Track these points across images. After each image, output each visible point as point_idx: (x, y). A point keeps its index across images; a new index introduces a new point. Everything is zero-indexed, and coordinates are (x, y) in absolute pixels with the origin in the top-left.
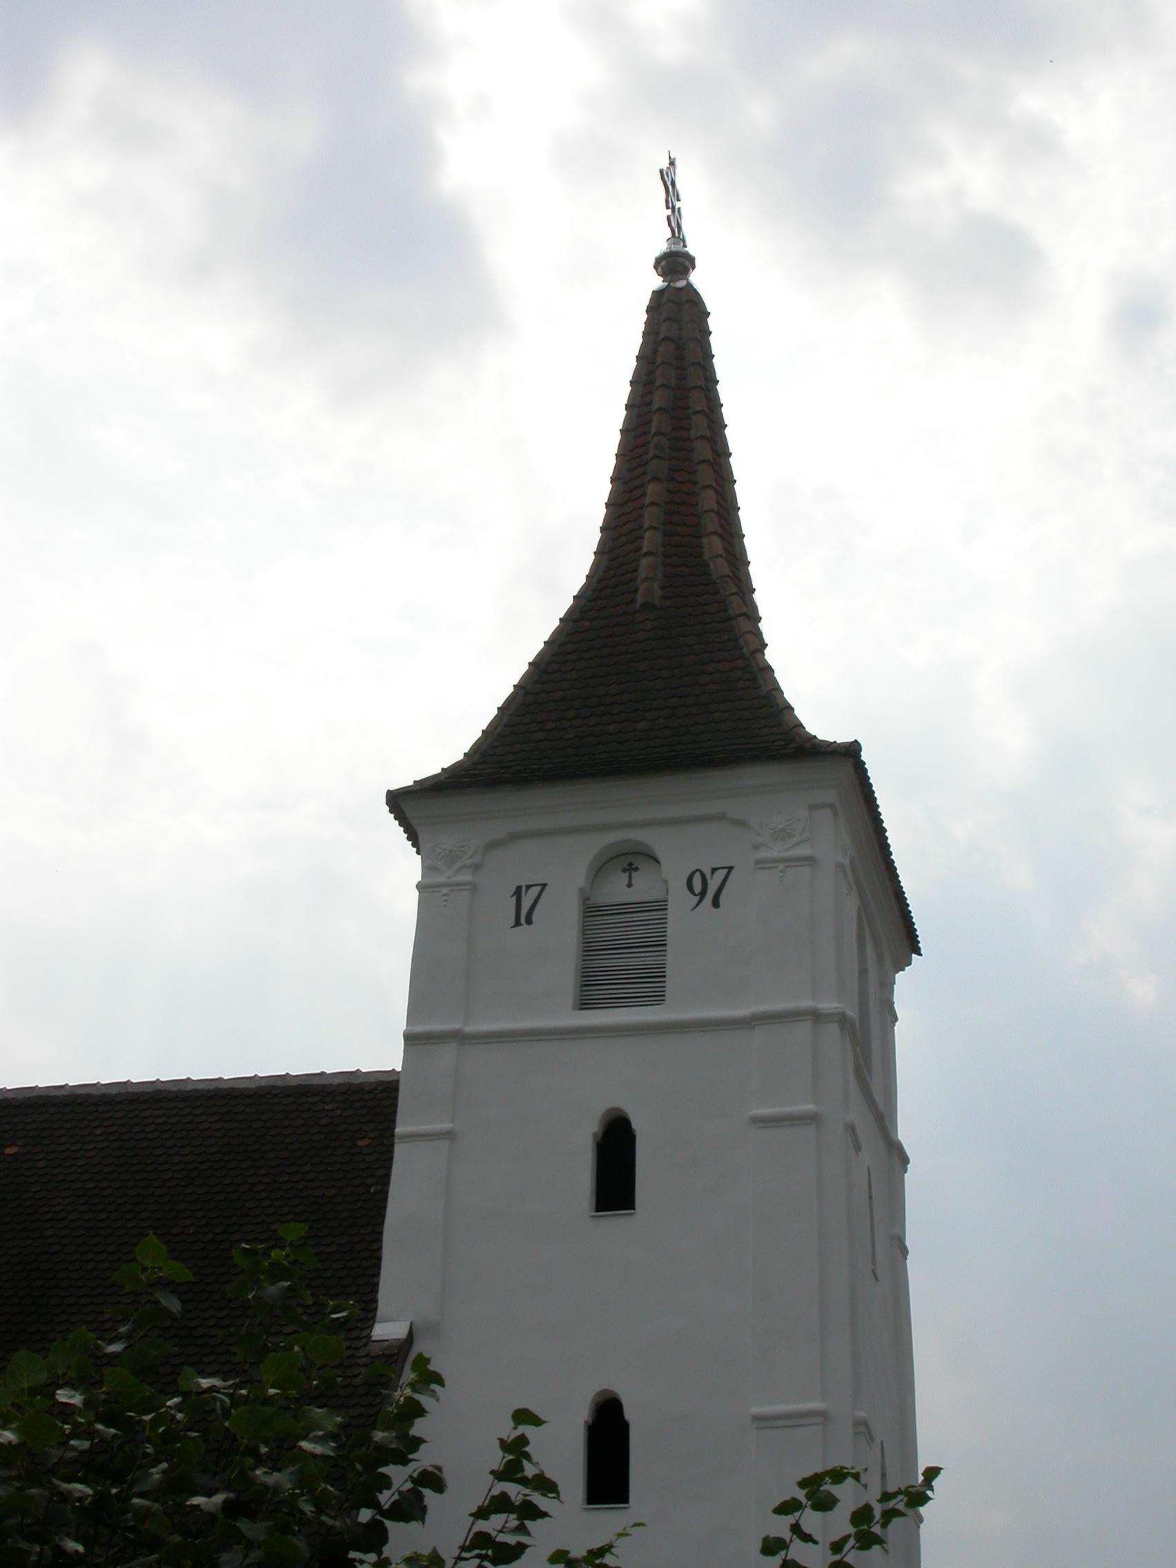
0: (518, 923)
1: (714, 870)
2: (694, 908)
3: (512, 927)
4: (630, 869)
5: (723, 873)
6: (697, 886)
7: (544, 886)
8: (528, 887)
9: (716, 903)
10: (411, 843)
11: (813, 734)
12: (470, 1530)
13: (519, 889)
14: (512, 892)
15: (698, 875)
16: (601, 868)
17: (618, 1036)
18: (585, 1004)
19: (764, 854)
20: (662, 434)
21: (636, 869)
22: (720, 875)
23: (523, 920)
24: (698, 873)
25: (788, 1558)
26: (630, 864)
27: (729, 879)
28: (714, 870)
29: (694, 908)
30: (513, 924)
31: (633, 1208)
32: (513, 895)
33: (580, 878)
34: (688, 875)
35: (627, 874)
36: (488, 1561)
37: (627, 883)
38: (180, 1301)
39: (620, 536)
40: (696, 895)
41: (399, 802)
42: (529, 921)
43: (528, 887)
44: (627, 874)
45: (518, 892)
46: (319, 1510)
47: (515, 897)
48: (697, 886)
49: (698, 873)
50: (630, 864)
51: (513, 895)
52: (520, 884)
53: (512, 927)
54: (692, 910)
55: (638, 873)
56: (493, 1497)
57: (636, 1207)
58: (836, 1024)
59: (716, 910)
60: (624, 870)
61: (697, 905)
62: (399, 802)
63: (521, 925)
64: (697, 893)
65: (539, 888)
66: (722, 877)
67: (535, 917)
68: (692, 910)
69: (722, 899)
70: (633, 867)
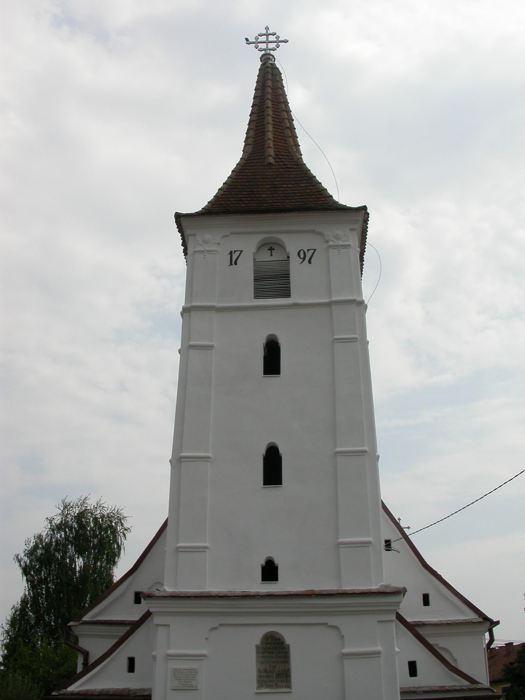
0: (231, 264)
1: (308, 250)
3: (229, 266)
4: (271, 249)
5: (312, 251)
6: (302, 256)
7: (242, 251)
8: (235, 251)
9: (310, 262)
14: (229, 252)
16: (260, 247)
17: (229, 311)
18: (257, 296)
20: (249, 144)
21: (274, 249)
22: (311, 252)
23: (233, 263)
24: (302, 251)
25: (498, 643)
26: (271, 247)
28: (308, 250)
30: (229, 264)
32: (229, 254)
33: (254, 250)
34: (298, 251)
37: (270, 254)
38: (131, 690)
42: (236, 264)
43: (235, 251)
46: (94, 547)
47: (230, 255)
48: (302, 256)
50: (271, 247)
51: (229, 254)
52: (231, 250)
53: (229, 266)
54: (300, 264)
55: (274, 250)
59: (310, 265)
60: (269, 249)
61: (302, 263)
62: (179, 217)
63: (232, 265)
67: (238, 262)
68: (300, 264)
69: (312, 261)
70: (272, 248)
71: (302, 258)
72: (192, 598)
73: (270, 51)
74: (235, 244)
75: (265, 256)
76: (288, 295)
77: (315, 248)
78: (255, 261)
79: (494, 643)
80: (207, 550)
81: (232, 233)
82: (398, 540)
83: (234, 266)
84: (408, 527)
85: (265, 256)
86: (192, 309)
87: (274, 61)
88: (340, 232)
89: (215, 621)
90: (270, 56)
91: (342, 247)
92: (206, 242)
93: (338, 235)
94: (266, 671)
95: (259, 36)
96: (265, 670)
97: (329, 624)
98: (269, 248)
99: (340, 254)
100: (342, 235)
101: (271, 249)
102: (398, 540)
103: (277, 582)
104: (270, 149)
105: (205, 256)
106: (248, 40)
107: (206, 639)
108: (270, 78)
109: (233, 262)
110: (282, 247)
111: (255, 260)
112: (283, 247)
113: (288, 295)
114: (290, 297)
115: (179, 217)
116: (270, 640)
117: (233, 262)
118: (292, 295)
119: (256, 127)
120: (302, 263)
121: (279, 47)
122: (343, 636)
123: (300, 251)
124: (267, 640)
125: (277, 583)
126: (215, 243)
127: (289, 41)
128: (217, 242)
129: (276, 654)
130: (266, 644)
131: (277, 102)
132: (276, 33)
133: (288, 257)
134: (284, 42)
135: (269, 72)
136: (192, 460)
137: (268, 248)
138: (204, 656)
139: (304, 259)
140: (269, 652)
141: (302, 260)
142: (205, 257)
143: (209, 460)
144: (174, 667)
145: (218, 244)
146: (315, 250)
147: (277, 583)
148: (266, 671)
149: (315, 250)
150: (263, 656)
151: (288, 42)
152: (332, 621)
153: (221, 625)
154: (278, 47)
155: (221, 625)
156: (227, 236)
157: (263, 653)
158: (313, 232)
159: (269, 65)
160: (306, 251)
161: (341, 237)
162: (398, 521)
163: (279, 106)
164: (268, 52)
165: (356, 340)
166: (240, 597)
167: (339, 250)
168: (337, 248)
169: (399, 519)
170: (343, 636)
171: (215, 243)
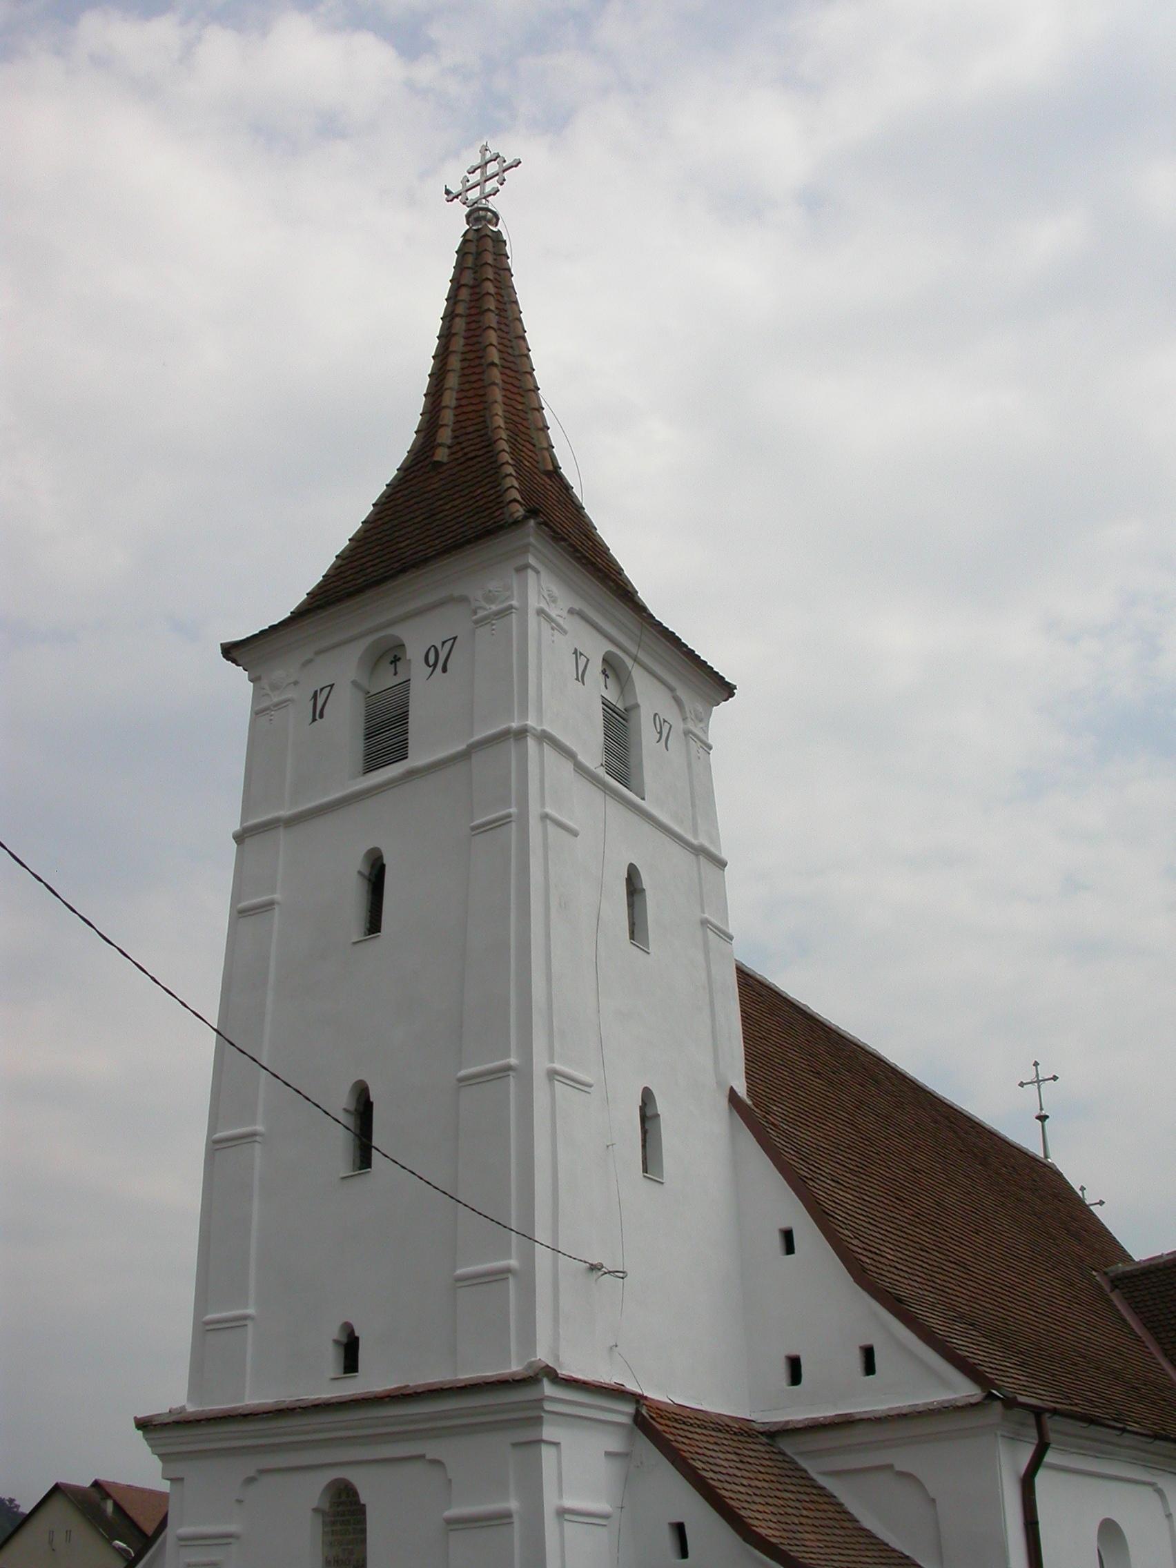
1: (444, 643)
6: (432, 660)
9: (444, 670)
12: (365, 940)
13: (316, 692)
15: (433, 651)
19: (481, 614)
23: (317, 717)
27: (455, 646)
35: (393, 665)
36: (1134, 1261)
39: (473, 307)
40: (430, 667)
41: (606, 1452)
42: (321, 716)
43: (322, 690)
47: (313, 700)
48: (432, 660)
49: (433, 648)
55: (401, 661)
56: (1016, 1397)
60: (391, 663)
61: (431, 675)
62: (606, 1452)
65: (329, 688)
66: (449, 647)
72: (203, 1422)
73: (486, 200)
80: (248, 1322)
81: (318, 653)
83: (319, 721)
84: (1101, 1201)
86: (245, 835)
88: (493, 585)
89: (249, 1465)
90: (481, 212)
91: (496, 617)
93: (490, 591)
94: (337, 1561)
95: (469, 173)
96: (336, 1559)
97: (897, 1468)
99: (493, 634)
100: (496, 589)
103: (356, 1374)
104: (497, 417)
105: (272, 718)
106: (451, 193)
107: (239, 1501)
108: (490, 261)
109: (318, 714)
111: (369, 693)
114: (406, 758)
116: (344, 1498)
117: (318, 714)
118: (409, 755)
120: (431, 675)
121: (505, 183)
122: (450, 1481)
124: (340, 1497)
125: (355, 1376)
126: (290, 684)
127: (521, 160)
128: (292, 680)
129: (354, 1524)
130: (338, 1506)
131: (478, 314)
132: (498, 153)
134: (512, 167)
135: (488, 251)
136: (230, 1144)
137: (390, 661)
138: (229, 1536)
139: (435, 665)
140: (343, 1521)
141: (431, 669)
142: (271, 720)
143: (257, 1138)
144: (188, 1560)
145: (296, 683)
147: (355, 1376)
148: (337, 1561)
150: (333, 1531)
151: (520, 162)
152: (431, 1449)
153: (263, 1472)
154: (502, 184)
155: (263, 1472)
156: (310, 661)
157: (333, 1523)
159: (490, 234)
161: (497, 593)
162: (1080, 1193)
164: (481, 203)
165: (508, 820)
166: (271, 1415)
167: (493, 625)
168: (489, 621)
169: (1082, 1189)
170: (933, 1500)
171: (290, 684)
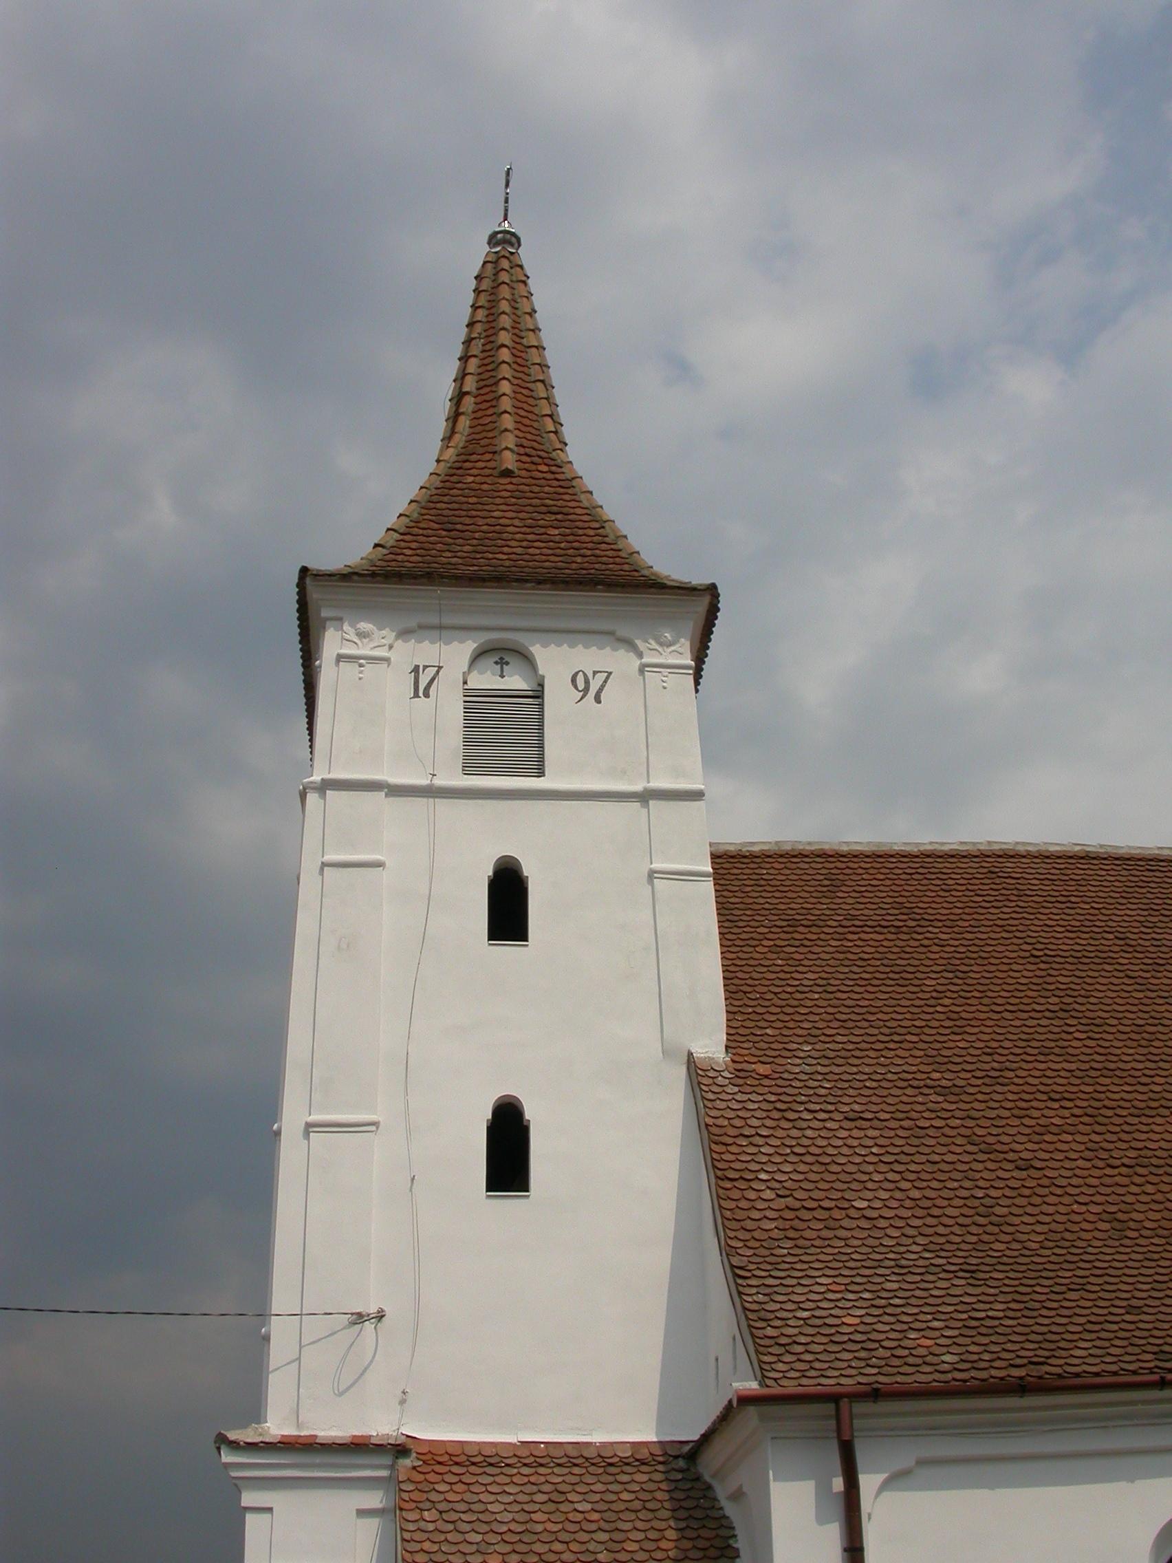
0: (416, 695)
1: (595, 673)
2: (579, 701)
4: (502, 663)
6: (581, 686)
8: (425, 667)
9: (598, 699)
10: (709, 644)
11: (727, 1403)
13: (417, 667)
16: (479, 656)
18: (469, 768)
21: (507, 663)
23: (421, 694)
26: (501, 659)
29: (579, 701)
30: (412, 696)
31: (526, 940)
35: (499, 666)
42: (427, 695)
43: (425, 667)
44: (499, 666)
45: (416, 670)
47: (413, 674)
57: (530, 939)
58: (853, 1404)
60: (496, 663)
64: (580, 689)
69: (603, 695)
71: (580, 689)
74: (426, 651)
75: (487, 679)
76: (541, 773)
77: (609, 670)
78: (466, 687)
79: (273, 1364)
82: (506, 201)
85: (487, 679)
87: (517, 249)
92: (362, 635)
98: (497, 659)
101: (502, 663)
102: (506, 201)
109: (421, 691)
110: (527, 659)
112: (526, 657)
113: (541, 773)
115: (304, 571)
119: (476, 403)
123: (577, 673)
133: (542, 685)
139: (586, 690)
146: (610, 673)
149: (610, 673)
158: (611, 633)
160: (590, 676)
163: (523, 338)
